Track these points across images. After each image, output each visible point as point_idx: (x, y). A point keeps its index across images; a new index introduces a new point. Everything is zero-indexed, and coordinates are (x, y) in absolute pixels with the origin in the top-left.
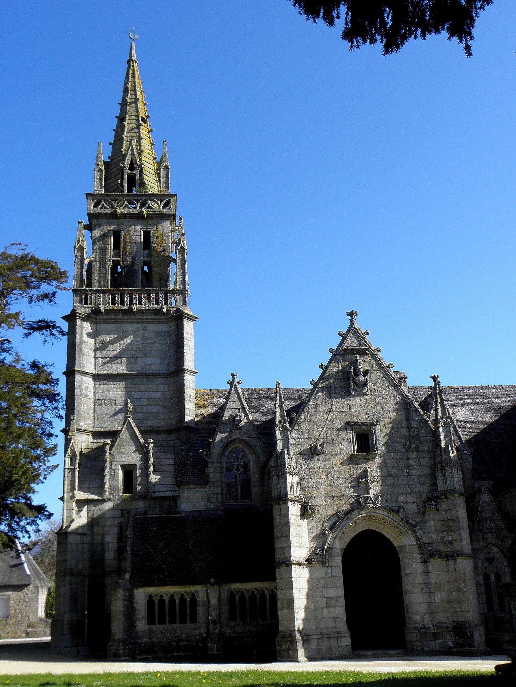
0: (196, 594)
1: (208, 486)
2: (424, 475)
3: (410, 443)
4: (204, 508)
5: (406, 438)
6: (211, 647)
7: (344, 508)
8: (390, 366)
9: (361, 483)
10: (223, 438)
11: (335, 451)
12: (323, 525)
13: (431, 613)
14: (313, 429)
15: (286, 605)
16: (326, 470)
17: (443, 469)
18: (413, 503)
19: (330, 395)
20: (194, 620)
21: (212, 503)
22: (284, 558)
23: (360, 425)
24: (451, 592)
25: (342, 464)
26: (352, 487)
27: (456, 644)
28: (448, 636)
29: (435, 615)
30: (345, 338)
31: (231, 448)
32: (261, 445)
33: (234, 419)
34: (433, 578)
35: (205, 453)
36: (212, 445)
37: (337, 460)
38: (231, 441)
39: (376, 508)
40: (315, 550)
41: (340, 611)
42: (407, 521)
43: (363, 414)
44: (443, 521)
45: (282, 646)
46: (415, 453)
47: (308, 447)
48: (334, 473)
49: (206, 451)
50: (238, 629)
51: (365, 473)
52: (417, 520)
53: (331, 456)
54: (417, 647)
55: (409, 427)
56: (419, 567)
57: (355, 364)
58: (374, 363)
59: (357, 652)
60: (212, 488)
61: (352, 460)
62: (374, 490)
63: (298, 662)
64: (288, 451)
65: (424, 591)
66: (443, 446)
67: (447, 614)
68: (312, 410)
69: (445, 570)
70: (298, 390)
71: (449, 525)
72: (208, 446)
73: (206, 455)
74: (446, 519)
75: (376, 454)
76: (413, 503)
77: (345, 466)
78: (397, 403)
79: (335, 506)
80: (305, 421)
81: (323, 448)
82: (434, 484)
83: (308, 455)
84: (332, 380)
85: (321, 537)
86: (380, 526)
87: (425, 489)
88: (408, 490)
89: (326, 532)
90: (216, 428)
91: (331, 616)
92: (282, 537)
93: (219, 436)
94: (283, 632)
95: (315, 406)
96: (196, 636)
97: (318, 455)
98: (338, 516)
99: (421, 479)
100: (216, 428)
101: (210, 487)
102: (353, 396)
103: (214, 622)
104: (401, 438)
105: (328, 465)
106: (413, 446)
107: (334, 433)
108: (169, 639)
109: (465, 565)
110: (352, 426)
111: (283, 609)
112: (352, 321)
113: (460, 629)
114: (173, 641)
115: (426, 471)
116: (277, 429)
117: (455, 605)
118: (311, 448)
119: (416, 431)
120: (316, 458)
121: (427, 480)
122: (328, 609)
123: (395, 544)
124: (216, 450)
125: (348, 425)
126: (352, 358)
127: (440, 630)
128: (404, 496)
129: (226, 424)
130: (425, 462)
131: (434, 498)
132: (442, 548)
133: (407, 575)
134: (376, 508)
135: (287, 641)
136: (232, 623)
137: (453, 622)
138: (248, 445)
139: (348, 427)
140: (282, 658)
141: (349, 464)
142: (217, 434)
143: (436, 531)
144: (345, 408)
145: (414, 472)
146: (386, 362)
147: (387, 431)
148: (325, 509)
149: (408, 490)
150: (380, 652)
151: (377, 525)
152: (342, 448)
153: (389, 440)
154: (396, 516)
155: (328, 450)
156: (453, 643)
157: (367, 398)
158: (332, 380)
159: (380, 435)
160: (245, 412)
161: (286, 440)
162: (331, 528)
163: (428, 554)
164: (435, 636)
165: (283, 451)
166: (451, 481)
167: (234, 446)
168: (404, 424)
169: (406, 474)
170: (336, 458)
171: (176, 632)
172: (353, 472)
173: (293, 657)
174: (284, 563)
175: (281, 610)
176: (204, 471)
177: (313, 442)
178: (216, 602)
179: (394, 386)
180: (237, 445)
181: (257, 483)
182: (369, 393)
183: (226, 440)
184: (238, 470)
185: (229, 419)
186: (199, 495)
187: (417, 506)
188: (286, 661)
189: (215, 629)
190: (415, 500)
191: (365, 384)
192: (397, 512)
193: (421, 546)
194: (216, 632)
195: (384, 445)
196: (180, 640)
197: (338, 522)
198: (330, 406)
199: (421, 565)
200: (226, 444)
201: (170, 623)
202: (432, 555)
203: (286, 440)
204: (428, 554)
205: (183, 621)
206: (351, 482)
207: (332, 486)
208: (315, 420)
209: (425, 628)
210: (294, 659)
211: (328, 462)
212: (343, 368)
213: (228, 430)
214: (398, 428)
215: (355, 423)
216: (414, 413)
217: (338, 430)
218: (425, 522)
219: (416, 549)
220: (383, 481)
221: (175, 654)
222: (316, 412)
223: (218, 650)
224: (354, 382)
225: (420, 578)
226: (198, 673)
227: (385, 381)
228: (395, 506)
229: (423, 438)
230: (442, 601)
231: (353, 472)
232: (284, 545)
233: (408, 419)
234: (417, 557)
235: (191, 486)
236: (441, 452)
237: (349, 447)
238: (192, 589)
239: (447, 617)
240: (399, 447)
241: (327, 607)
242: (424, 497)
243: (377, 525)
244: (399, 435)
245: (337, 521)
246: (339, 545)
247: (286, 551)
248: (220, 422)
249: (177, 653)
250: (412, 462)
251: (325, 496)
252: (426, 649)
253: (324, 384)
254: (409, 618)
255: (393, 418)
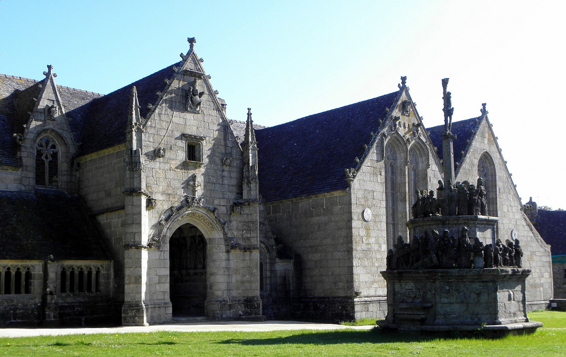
0: (32, 268)
1: (20, 169)
2: (232, 185)
3: (226, 159)
4: (16, 190)
5: (222, 154)
6: (49, 314)
7: (176, 205)
8: (216, 92)
9: (190, 185)
10: (37, 127)
11: (172, 157)
12: (160, 217)
13: (229, 290)
14: (157, 134)
15: (133, 280)
16: (165, 171)
17: (249, 183)
18: (224, 206)
19: (171, 108)
20: (28, 291)
21: (25, 185)
22: (134, 242)
23: (192, 138)
24: (245, 275)
25: (177, 168)
26: (183, 188)
27: (246, 313)
28: (239, 307)
29: (231, 291)
30: (186, 61)
31: (42, 137)
32: (71, 138)
33: (49, 110)
34: (232, 264)
35: (18, 137)
36: (26, 131)
37: (175, 164)
38: (44, 130)
39: (199, 207)
40: (153, 237)
41: (166, 287)
42: (219, 221)
43: (194, 128)
44: (244, 222)
45: (127, 314)
46: (228, 167)
47: (152, 149)
48: (171, 175)
49: (20, 136)
50: (69, 300)
51: (194, 178)
52: (225, 220)
53: (169, 160)
54: (218, 314)
55: (226, 146)
56: (223, 255)
57: (193, 84)
58: (205, 88)
59: (175, 318)
60: (25, 172)
61: (184, 166)
62: (199, 191)
63: (144, 326)
64: (142, 150)
65: (225, 273)
66: (251, 165)
67: (240, 291)
68: (157, 118)
69: (241, 259)
70: (81, 92)
71: (248, 226)
72: (22, 131)
73: (20, 140)
74: (247, 220)
75: (203, 164)
76: (224, 206)
77: (179, 170)
78: (219, 125)
79: (170, 202)
80: (151, 126)
81: (165, 152)
82: (240, 193)
83: (152, 157)
84: (173, 95)
85: (158, 226)
86: (198, 221)
87: (232, 196)
88: (221, 196)
89: (163, 222)
90: (30, 115)
91: (162, 290)
92: (133, 224)
93: (34, 124)
94: (129, 302)
95: (160, 114)
96: (31, 305)
97: (160, 157)
98: (172, 210)
99: (231, 188)
100: (30, 115)
101: (23, 170)
102: (188, 112)
103: (51, 293)
104: (219, 153)
105: (166, 168)
106: (228, 161)
107: (173, 141)
108: (6, 308)
109: (256, 255)
110: (186, 137)
111: (130, 283)
112: (191, 46)
113: (249, 302)
114: (11, 310)
115: (234, 182)
116: (133, 129)
117: (247, 285)
118: (155, 151)
119: (230, 150)
120: (158, 160)
121: (234, 189)
122: (160, 285)
123: (206, 236)
124: (30, 136)
125: (184, 136)
126: (192, 79)
127: (234, 302)
128: (218, 200)
129: (41, 113)
130: (234, 175)
131: (238, 204)
132: (241, 242)
133: (214, 261)
134: (199, 207)
135: (133, 310)
136: (64, 295)
137: (244, 297)
138: (60, 137)
139: (183, 138)
140: (127, 323)
141: (182, 169)
142: (32, 121)
143: (237, 229)
144: (181, 121)
145: (226, 182)
146: (214, 89)
147: (211, 146)
148: (163, 205)
149: (221, 196)
150: (191, 318)
151: (196, 220)
152: (178, 154)
153: (211, 153)
154: (212, 215)
155: (167, 155)
156: (243, 312)
157: (199, 116)
158: (173, 95)
159: (206, 148)
160: (59, 104)
161: (140, 140)
162: (167, 220)
163: (231, 246)
164: (230, 307)
165: (137, 150)
166: (254, 192)
167: (45, 135)
168: (223, 143)
169: (221, 183)
170: (173, 162)
171: (12, 301)
172: (185, 175)
173: (139, 322)
174: (134, 246)
175: (128, 284)
176: (15, 154)
177: (156, 145)
178: (55, 276)
179: (218, 110)
180: (48, 134)
181: (65, 173)
182: (200, 112)
183: (40, 129)
184: (47, 157)
185: (44, 109)
186: (12, 177)
187: (226, 209)
188: (132, 326)
189: (52, 299)
190: (225, 204)
191: (199, 104)
192: (213, 212)
193: (227, 240)
194: (53, 302)
195: (207, 157)
196: (16, 309)
197: (172, 215)
198: (171, 117)
199: (225, 254)
200: (40, 132)
201: (6, 293)
202: (233, 247)
203: (140, 140)
204: (231, 246)
205: (18, 291)
206: (182, 184)
207: (169, 186)
208: (159, 127)
209: (224, 301)
210: (142, 324)
211: (166, 165)
212: (183, 86)
213: (43, 119)
214: (218, 145)
215: (189, 135)
216: (230, 135)
217: (176, 139)
218: (230, 222)
219: (223, 242)
220: (205, 186)
221: (12, 321)
222: (160, 120)
223: (55, 317)
224: (192, 101)
225: (224, 264)
226: (133, 334)
227: (212, 104)
228: (212, 207)
229: (234, 156)
230: (237, 281)
231: (185, 175)
232: (135, 231)
233: (225, 139)
234: (223, 247)
235: (6, 167)
236: (248, 169)
237: (182, 156)
238: (29, 263)
239: (239, 293)
240: (218, 160)
241: (159, 283)
242: (231, 203)
243: (196, 220)
244: (219, 151)
245: (171, 214)
246: (169, 235)
247: (137, 237)
248: (35, 110)
249: (14, 319)
250: (225, 174)
251: (163, 193)
252: (224, 316)
253: (167, 97)
254: (212, 293)
255: (215, 137)
